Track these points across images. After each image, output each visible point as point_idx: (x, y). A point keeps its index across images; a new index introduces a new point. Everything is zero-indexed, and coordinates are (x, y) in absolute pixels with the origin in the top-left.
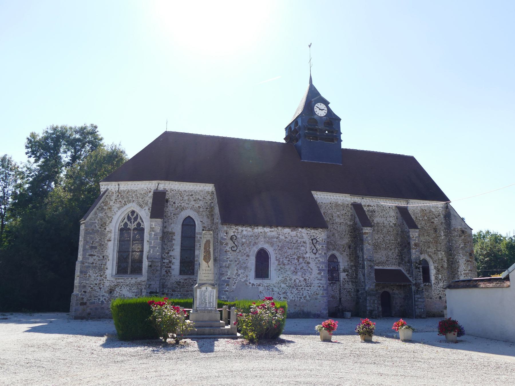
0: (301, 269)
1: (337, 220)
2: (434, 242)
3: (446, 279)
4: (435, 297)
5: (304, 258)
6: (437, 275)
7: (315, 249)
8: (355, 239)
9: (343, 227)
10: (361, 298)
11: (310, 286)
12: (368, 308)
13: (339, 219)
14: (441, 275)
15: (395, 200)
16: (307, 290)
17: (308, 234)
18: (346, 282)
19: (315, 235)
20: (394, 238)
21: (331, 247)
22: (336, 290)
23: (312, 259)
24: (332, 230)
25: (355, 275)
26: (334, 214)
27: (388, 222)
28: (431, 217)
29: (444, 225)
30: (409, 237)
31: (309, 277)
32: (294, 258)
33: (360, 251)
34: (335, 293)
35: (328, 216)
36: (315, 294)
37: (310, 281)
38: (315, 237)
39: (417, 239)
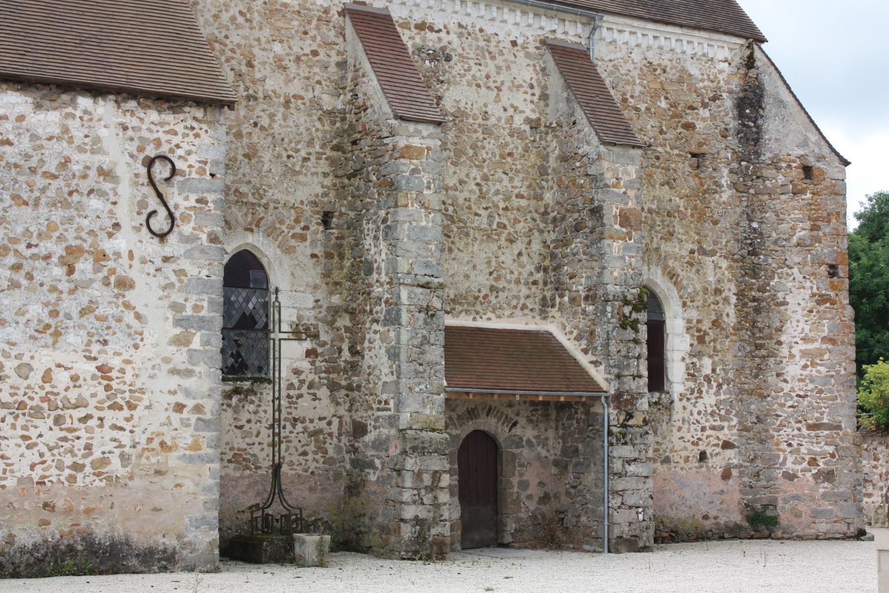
0: (83, 313)
2: (692, 215)
3: (731, 375)
4: (684, 454)
5: (101, 257)
6: (695, 360)
7: (162, 212)
8: (356, 181)
10: (371, 465)
11: (132, 407)
12: (409, 512)
13: (283, 77)
14: (710, 361)
15: (542, 11)
16: (115, 427)
17: (130, 133)
18: (305, 387)
19: (164, 138)
20: (529, 187)
21: (237, 213)
22: (254, 427)
23: (143, 261)
24: (244, 132)
25: (346, 354)
26: (256, 51)
27: (505, 110)
29: (733, 141)
31: (126, 356)
32: (47, 257)
33: (376, 238)
34: (248, 440)
35: (227, 61)
36: (155, 444)
37: (128, 377)
38: (164, 149)
39: (631, 193)
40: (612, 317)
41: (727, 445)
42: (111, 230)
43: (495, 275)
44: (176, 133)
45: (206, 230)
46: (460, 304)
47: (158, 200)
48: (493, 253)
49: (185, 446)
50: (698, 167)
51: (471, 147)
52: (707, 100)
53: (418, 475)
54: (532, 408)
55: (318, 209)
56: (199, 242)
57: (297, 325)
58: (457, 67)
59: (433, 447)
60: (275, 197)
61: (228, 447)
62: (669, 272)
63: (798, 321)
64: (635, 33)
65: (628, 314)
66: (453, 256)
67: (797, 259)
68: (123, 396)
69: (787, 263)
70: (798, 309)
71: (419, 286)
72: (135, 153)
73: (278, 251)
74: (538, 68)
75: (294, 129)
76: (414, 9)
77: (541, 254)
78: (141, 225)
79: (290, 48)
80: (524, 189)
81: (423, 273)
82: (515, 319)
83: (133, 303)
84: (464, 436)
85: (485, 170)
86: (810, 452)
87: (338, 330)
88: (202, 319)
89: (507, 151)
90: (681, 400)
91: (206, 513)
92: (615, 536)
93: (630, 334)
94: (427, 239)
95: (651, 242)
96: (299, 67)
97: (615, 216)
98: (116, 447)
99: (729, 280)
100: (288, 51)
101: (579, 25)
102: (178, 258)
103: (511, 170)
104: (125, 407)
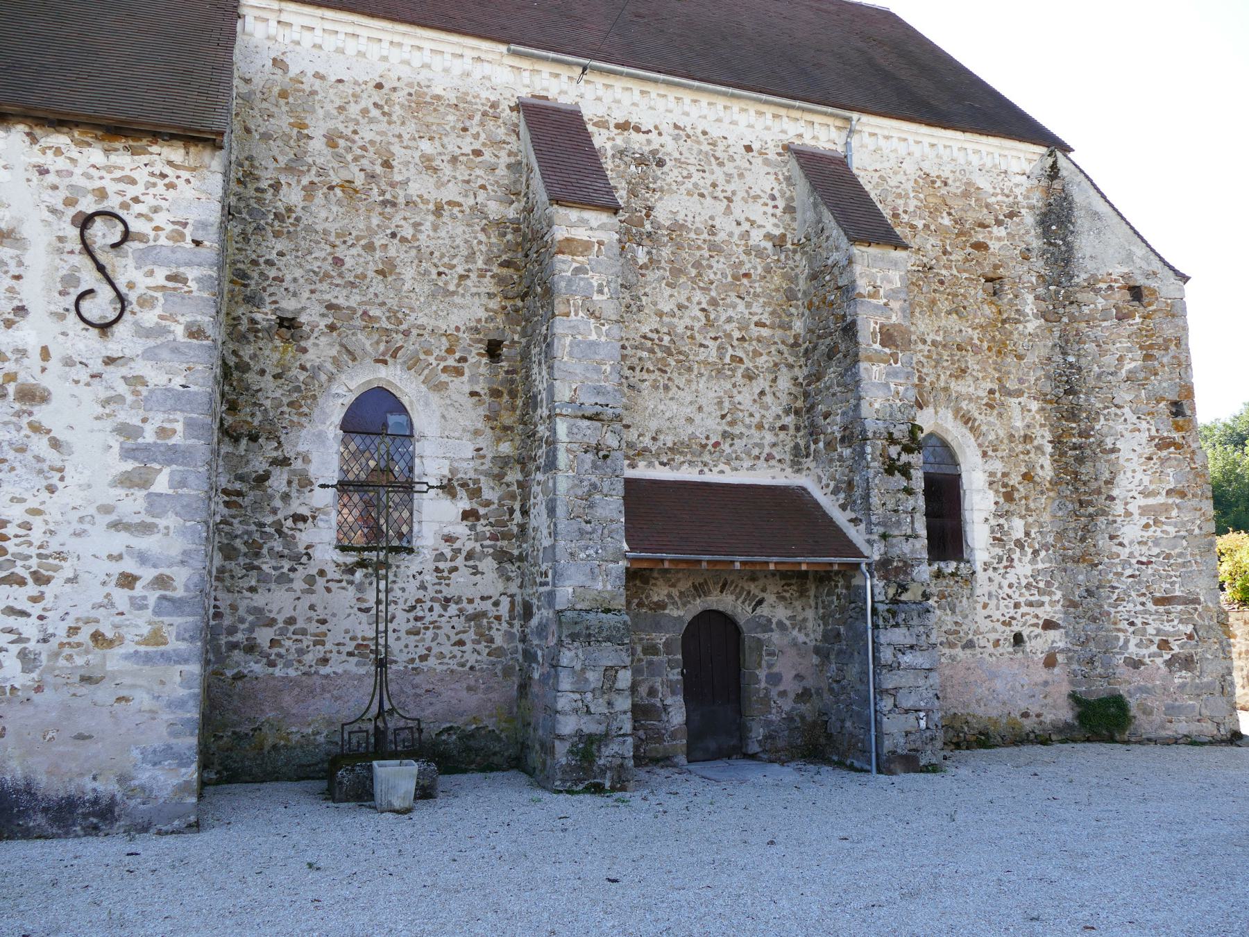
1: (421, 186)
2: (990, 349)
3: (1050, 539)
4: (993, 636)
6: (1002, 521)
7: (105, 293)
9: (456, 230)
12: (568, 725)
14: (1022, 522)
15: (783, 112)
17: (51, 178)
19: (111, 187)
20: (772, 313)
24: (377, 244)
25: (517, 515)
26: (396, 149)
27: (739, 224)
28: (971, 217)
29: (1039, 264)
30: (848, 291)
31: (33, 503)
35: (356, 159)
36: (84, 636)
37: (37, 536)
38: (112, 204)
39: (896, 305)
40: (873, 459)
41: (1049, 625)
42: (11, 316)
43: (729, 418)
44: (133, 182)
45: (182, 319)
46: (681, 453)
47: (99, 275)
48: (725, 392)
49: (137, 638)
50: (995, 294)
51: (693, 266)
52: (1001, 217)
53: (580, 676)
54: (783, 582)
55: (481, 336)
56: (171, 337)
57: (450, 480)
58: (672, 173)
59: (604, 634)
60: (419, 322)
61: (348, 636)
62: (963, 416)
63: (1134, 471)
64: (905, 140)
65: (895, 456)
66: (670, 395)
67: (1128, 397)
68: (27, 563)
69: (1115, 401)
70: (1132, 455)
71: (584, 417)
72: (60, 207)
73: (423, 388)
74: (781, 177)
75: (447, 241)
76: (614, 106)
77: (790, 394)
78: (67, 310)
79: (443, 146)
80: (766, 315)
81: (593, 401)
82: (758, 472)
83: (46, 424)
84: (689, 618)
85: (713, 294)
86: (1159, 632)
87: (508, 486)
88: (174, 449)
89: (743, 271)
90: (985, 570)
91: (173, 741)
92: (885, 751)
93: (899, 481)
94: (598, 357)
95: (938, 379)
96: (455, 169)
97: (874, 333)
98: (12, 642)
99: (1042, 425)
100: (440, 149)
101: (833, 129)
102: (132, 359)
103: (748, 293)
104: (30, 581)
